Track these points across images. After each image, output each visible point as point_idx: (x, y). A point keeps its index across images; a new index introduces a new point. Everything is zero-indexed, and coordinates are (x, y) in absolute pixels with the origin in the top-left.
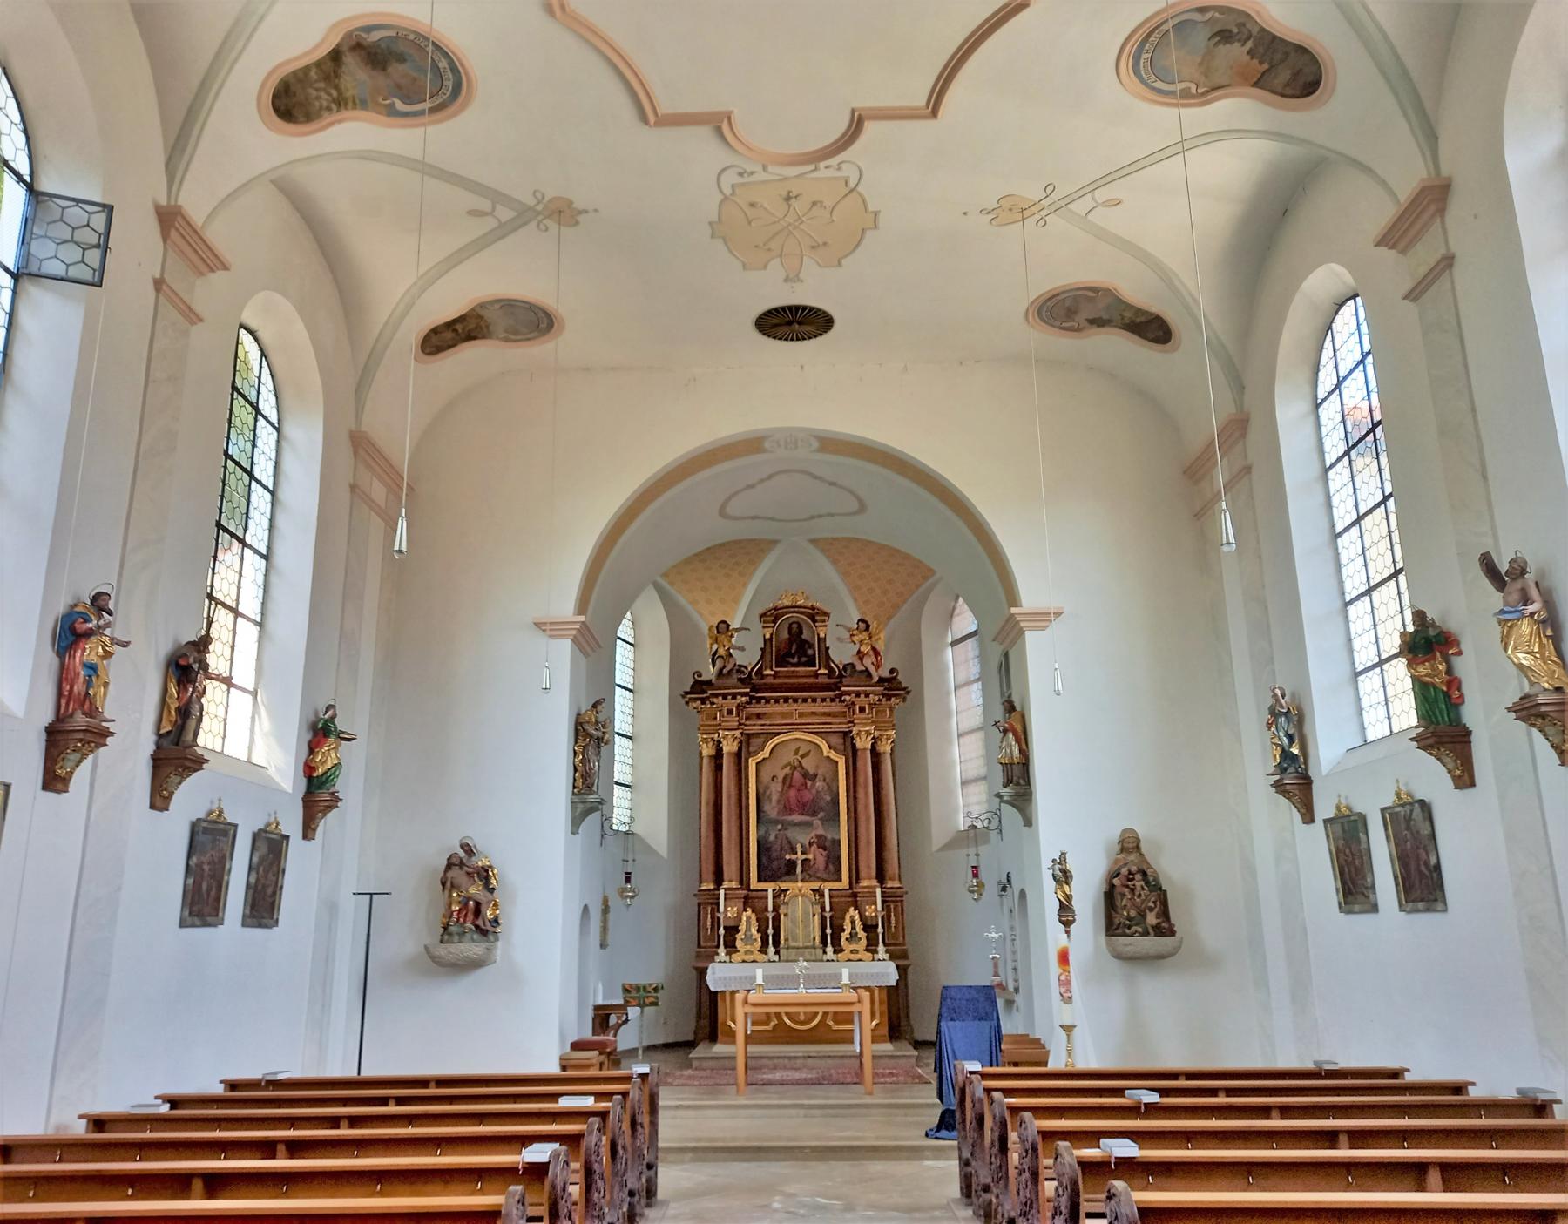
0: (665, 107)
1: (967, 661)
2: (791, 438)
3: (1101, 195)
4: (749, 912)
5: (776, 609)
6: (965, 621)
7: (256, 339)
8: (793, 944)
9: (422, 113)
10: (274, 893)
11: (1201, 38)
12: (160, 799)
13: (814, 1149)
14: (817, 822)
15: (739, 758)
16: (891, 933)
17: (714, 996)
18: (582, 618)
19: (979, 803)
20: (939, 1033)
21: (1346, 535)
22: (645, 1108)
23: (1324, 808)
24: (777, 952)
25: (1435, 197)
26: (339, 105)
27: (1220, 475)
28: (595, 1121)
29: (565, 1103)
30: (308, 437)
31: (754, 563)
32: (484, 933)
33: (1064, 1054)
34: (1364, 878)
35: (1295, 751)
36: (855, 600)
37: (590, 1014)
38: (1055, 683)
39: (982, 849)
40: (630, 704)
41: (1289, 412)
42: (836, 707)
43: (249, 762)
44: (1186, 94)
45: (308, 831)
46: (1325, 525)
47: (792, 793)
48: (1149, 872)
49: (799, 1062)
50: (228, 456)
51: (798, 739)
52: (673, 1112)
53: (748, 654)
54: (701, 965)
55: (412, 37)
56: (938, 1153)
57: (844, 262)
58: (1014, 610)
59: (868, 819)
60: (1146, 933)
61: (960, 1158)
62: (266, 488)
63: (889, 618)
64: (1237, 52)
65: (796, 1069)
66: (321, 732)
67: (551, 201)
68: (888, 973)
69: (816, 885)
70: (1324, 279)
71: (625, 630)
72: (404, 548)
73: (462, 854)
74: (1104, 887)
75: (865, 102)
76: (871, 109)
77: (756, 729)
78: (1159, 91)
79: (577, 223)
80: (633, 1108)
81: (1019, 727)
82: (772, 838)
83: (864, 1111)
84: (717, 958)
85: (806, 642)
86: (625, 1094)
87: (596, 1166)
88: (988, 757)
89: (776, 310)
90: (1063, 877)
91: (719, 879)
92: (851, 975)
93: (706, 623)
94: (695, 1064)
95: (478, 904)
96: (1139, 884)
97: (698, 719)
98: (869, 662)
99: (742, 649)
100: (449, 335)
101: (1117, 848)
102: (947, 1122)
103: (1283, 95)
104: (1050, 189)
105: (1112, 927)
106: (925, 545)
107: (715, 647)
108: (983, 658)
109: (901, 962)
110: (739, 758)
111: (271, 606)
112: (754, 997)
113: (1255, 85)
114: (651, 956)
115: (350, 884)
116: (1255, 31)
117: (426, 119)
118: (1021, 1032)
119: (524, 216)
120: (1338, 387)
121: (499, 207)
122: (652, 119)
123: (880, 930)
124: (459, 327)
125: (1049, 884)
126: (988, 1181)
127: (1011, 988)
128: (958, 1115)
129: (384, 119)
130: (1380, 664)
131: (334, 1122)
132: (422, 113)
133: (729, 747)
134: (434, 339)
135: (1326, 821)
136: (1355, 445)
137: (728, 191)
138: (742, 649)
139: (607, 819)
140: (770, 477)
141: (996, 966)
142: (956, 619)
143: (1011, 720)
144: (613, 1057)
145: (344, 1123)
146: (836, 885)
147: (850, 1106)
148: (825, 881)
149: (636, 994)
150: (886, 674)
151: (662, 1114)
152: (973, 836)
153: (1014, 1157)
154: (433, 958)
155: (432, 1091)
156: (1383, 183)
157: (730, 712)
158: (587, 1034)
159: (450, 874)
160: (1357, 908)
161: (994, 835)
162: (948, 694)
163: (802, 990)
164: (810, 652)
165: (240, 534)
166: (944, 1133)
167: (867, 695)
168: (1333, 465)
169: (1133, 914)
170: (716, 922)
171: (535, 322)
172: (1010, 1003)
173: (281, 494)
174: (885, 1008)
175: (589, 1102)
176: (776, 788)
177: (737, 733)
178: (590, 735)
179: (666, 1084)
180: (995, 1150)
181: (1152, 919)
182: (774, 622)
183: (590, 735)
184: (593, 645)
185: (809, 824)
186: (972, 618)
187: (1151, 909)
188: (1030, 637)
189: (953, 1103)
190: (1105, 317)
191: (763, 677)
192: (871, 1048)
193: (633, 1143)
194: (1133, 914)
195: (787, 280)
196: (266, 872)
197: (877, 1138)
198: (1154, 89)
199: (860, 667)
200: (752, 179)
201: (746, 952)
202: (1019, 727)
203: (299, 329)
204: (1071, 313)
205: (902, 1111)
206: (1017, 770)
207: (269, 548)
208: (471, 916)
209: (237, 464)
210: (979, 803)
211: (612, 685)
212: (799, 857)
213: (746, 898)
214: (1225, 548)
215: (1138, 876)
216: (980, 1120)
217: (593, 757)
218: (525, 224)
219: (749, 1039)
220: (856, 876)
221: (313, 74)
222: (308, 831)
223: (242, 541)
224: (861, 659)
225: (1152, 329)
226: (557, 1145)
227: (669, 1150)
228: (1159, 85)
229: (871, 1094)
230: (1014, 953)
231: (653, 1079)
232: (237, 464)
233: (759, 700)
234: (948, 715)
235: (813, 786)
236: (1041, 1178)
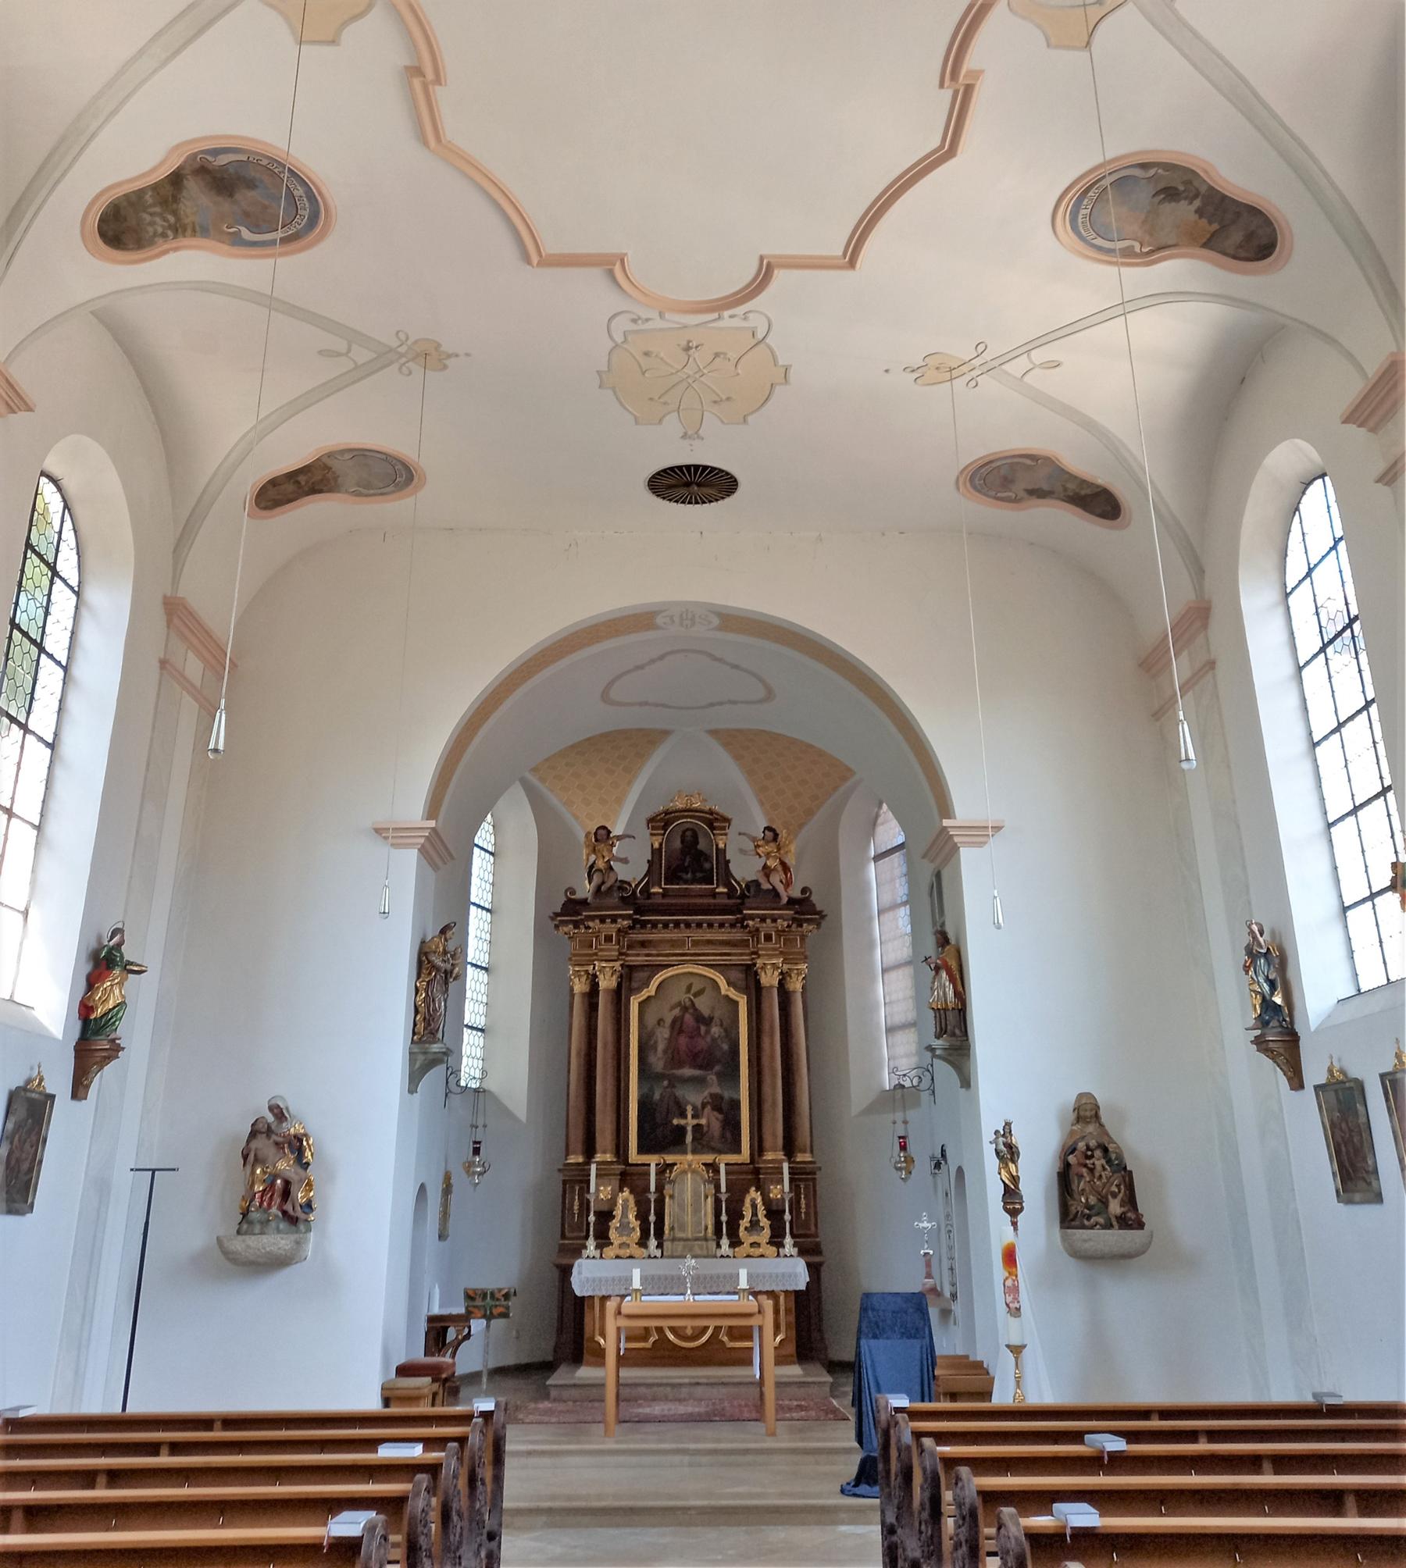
0: (550, 247)
1: (893, 880)
2: (688, 614)
3: (1038, 356)
4: (626, 1193)
5: (667, 813)
6: (890, 832)
7: (59, 489)
8: (679, 1235)
9: (273, 243)
10: (30, 1170)
11: (1144, 195)
13: (703, 1511)
14: (712, 1078)
15: (619, 997)
16: (803, 1225)
17: (582, 1300)
18: (432, 824)
19: (907, 1056)
20: (858, 1354)
21: (1324, 744)
22: (488, 1457)
23: (1314, 1073)
24: (660, 1246)
26: (176, 231)
27: (1178, 670)
28: (423, 1478)
29: (387, 1453)
30: (113, 606)
31: (642, 756)
32: (293, 1221)
33: (1012, 1383)
34: (1365, 1159)
35: (1278, 1000)
36: (762, 804)
37: (422, 1327)
38: (994, 912)
39: (912, 1114)
40: (487, 927)
41: (1255, 602)
42: (737, 935)
43: (11, 1000)
44: (1128, 253)
45: (79, 1089)
46: (1299, 731)
47: (683, 1040)
48: (1111, 1147)
49: (684, 1390)
50: (14, 625)
51: (691, 972)
52: (523, 1460)
53: (632, 866)
54: (565, 1261)
55: (264, 162)
56: (857, 1516)
57: (750, 418)
58: (946, 823)
59: (774, 1076)
60: (1108, 1226)
61: (883, 1524)
62: (58, 663)
63: (801, 826)
64: (1185, 211)
65: (680, 1400)
66: (104, 962)
67: (416, 342)
68: (793, 1272)
69: (709, 1158)
70: (1288, 456)
71: (484, 836)
72: (221, 747)
73: (270, 1118)
74: (1057, 1166)
75: (771, 250)
76: (780, 257)
77: (640, 960)
78: (1100, 249)
79: (445, 367)
80: (472, 1458)
81: (954, 965)
82: (657, 1096)
83: (760, 1458)
84: (585, 1253)
85: (701, 853)
86: (462, 1440)
87: (422, 1540)
88: (918, 998)
89: (672, 469)
90: (1009, 1153)
91: (590, 1151)
92: (750, 1276)
93: (581, 829)
94: (554, 1393)
95: (287, 1183)
96: (1099, 1162)
97: (570, 947)
98: (776, 879)
99: (625, 861)
100: (290, 487)
101: (1072, 1117)
102: (867, 1474)
103: (1235, 257)
104: (981, 348)
105: (1069, 1216)
106: (839, 743)
107: (593, 858)
108: (911, 876)
109: (816, 1259)
110: (619, 997)
111: (53, 805)
112: (629, 1305)
113: (1205, 245)
114: (503, 1260)
115: (127, 1158)
116: (1203, 189)
117: (278, 249)
118: (960, 1352)
119: (385, 358)
120: (1309, 574)
121: (354, 347)
122: (535, 259)
123: (787, 1217)
124: (302, 479)
125: (991, 1162)
126: (917, 1554)
127: (947, 1294)
128: (880, 1466)
129: (226, 247)
130: (1372, 896)
131: (87, 1478)
132: (273, 243)
133: (607, 982)
134: (272, 493)
135: (1316, 1088)
136: (1331, 641)
137: (619, 339)
138: (625, 861)
139: (456, 1072)
140: (662, 657)
141: (928, 1265)
142: (880, 830)
143: (944, 955)
144: (450, 1385)
145: (102, 1480)
146: (733, 1158)
147: (746, 1452)
148: (720, 1152)
149: (481, 1303)
150: (796, 893)
151: (509, 1462)
152: (900, 1097)
153: (949, 1524)
154: (226, 1253)
155: (217, 1435)
156: (1350, 356)
157: (609, 939)
158: (419, 1355)
159: (254, 1145)
160: (1357, 1197)
161: (925, 1096)
162: (870, 919)
163: (689, 1297)
164: (707, 865)
165: (22, 719)
166: (863, 1488)
167: (774, 921)
169: (1093, 1200)
170: (585, 1206)
171: (391, 475)
172: (946, 1313)
173: (77, 671)
174: (792, 1319)
175: (416, 1452)
176: (663, 1034)
177: (617, 965)
178: (437, 967)
179: (517, 1421)
180: (925, 1515)
181: (1115, 1207)
182: (665, 828)
183: (437, 967)
184: (445, 857)
185: (700, 1082)
186: (898, 829)
187: (1114, 1195)
188: (967, 855)
189: (876, 1441)
190: (1046, 487)
191: (649, 896)
192: (777, 1373)
193: (472, 1506)
194: (1093, 1200)
195: (685, 436)
196: (22, 1142)
197: (782, 1495)
198: (1094, 246)
199: (766, 886)
200: (649, 325)
201: (621, 1246)
202: (954, 965)
203: (111, 482)
204: (1007, 482)
205: (810, 1458)
206: (952, 1017)
208: (277, 1200)
209: (25, 634)
210: (907, 1056)
211: (465, 903)
212: (690, 1122)
213: (623, 1174)
214: (1185, 765)
215: (1098, 1153)
216: (907, 1475)
217: (439, 996)
218: (388, 365)
219: (622, 1361)
220: (758, 1148)
221: (149, 198)
222: (79, 1089)
223: (24, 727)
224: (767, 876)
225: (1100, 503)
226: (373, 1514)
227: (518, 1512)
228: (1099, 242)
229: (773, 1434)
230: (951, 1248)
231: (499, 1418)
232: (25, 634)
233: (644, 924)
234: (871, 946)
235: (708, 1032)
236: (982, 1553)
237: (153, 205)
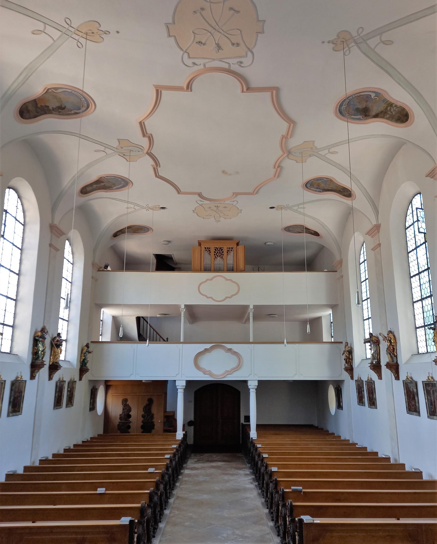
12: (50, 378)
23: (403, 376)
25: (377, 228)
45: (32, 377)
168: (410, 252)
207: (19, 271)
222: (80, 379)
237: (389, 114)
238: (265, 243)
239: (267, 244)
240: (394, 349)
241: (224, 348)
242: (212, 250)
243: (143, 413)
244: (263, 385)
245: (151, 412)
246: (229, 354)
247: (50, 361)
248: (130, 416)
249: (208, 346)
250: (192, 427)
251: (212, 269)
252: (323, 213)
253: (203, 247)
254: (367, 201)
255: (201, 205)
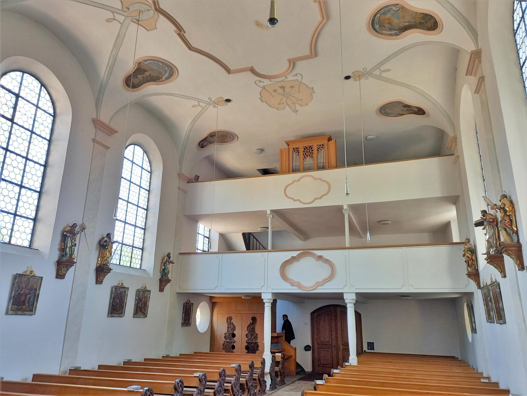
238: (366, 138)
239: (368, 137)
240: (511, 221)
241: (313, 255)
242: (301, 150)
243: (247, 332)
244: (363, 299)
245: (254, 332)
246: (320, 262)
247: (97, 263)
248: (234, 335)
249: (295, 254)
250: (310, 353)
251: (301, 169)
252: (414, 73)
253: (291, 147)
254: (469, 38)
255: (264, 88)
